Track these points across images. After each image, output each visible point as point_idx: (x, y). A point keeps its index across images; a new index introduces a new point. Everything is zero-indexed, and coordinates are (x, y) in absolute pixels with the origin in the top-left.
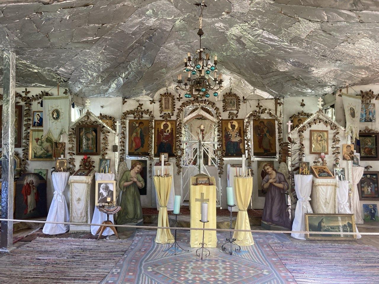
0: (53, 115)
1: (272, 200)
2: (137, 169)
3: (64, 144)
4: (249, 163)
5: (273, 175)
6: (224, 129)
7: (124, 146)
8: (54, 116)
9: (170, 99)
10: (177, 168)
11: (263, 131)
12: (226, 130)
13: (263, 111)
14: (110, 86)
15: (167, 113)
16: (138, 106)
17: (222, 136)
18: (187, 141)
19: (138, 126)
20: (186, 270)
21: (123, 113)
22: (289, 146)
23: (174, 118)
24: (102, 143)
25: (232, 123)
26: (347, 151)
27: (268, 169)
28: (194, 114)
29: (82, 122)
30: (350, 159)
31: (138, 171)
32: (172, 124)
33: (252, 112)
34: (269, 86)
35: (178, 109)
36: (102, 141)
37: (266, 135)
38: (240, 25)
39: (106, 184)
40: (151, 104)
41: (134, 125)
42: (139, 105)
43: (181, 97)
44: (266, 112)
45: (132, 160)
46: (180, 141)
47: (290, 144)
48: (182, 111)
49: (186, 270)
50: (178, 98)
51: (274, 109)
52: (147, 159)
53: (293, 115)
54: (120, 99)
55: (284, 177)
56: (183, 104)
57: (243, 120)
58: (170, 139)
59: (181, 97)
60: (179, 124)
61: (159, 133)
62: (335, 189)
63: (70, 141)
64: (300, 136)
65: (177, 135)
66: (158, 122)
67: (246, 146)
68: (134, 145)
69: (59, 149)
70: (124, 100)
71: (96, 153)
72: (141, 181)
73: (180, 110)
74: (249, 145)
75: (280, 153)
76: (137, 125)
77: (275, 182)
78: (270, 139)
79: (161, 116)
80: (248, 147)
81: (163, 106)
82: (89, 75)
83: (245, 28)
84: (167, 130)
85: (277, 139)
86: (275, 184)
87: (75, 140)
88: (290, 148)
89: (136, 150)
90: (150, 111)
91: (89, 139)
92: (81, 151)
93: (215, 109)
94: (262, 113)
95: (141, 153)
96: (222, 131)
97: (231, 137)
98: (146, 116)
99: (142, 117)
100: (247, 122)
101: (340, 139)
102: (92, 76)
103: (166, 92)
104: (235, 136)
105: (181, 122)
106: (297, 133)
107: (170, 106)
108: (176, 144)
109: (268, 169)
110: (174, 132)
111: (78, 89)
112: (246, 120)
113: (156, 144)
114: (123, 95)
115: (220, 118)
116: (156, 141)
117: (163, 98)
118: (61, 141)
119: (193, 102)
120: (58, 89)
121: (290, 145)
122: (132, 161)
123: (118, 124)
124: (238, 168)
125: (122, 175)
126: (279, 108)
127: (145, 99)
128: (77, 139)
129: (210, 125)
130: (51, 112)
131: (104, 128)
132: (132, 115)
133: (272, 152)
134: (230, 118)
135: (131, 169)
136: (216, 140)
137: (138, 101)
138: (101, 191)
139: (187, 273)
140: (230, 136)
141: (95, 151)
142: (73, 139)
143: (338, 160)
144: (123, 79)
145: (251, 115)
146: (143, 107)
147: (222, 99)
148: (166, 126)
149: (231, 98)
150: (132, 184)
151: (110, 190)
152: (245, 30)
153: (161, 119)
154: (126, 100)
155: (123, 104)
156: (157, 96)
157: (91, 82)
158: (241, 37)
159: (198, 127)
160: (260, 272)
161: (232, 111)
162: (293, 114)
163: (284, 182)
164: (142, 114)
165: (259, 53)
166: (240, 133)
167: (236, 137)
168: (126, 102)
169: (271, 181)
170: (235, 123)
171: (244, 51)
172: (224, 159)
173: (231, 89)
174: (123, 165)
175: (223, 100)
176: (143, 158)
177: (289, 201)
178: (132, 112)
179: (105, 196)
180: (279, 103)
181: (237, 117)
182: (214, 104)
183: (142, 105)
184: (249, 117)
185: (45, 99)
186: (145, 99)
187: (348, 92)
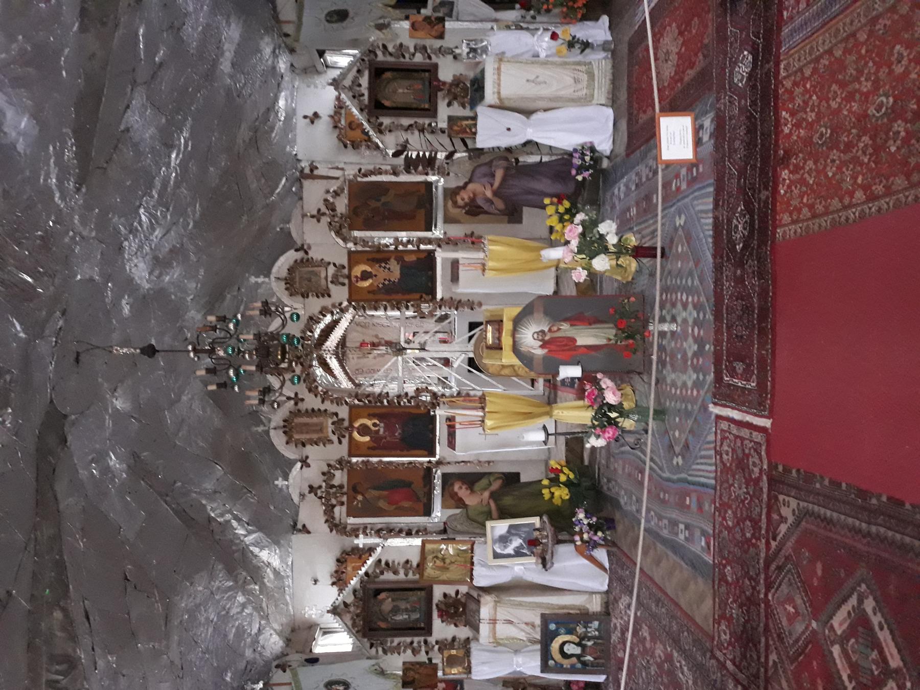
1: (532, 193)
4: (448, 242)
6: (371, 296)
13: (330, 207)
16: (316, 495)
17: (388, 301)
18: (395, 379)
19: (363, 495)
20: (679, 384)
21: (331, 531)
22: (414, 157)
23: (344, 412)
24: (406, 575)
25: (356, 277)
27: (463, 199)
28: (334, 363)
29: (354, 625)
30: (440, 25)
32: (359, 417)
33: (333, 234)
35: (323, 402)
37: (384, 204)
38: (130, 260)
39: (494, 542)
40: (309, 466)
42: (313, 494)
43: (293, 396)
44: (331, 200)
46: (399, 397)
49: (679, 384)
50: (296, 404)
51: (325, 182)
52: (439, 472)
53: (340, 139)
56: (310, 391)
57: (350, 253)
59: (293, 396)
61: (379, 446)
63: (397, 650)
65: (385, 403)
67: (410, 247)
68: (406, 504)
69: (417, 676)
70: (300, 531)
73: (325, 396)
74: (409, 242)
75: (427, 174)
76: (360, 498)
77: (492, 186)
79: (340, 442)
81: (315, 436)
82: (243, 611)
83: (134, 246)
85: (393, 178)
86: (497, 184)
87: (397, 640)
88: (418, 154)
89: (418, 500)
90: (326, 469)
91: (394, 606)
92: (422, 625)
94: (334, 210)
95: (425, 486)
97: (389, 281)
98: (340, 477)
99: (341, 487)
100: (355, 244)
102: (244, 606)
103: (281, 432)
105: (353, 394)
107: (315, 420)
108: (405, 407)
109: (463, 199)
110: (377, 411)
111: (275, 638)
112: (350, 245)
114: (287, 533)
115: (345, 304)
116: (398, 452)
117: (296, 436)
118: (401, 673)
120: (275, 685)
122: (444, 506)
123: (361, 541)
124: (461, 268)
125: (475, 525)
126: (322, 171)
127: (296, 481)
128: (396, 636)
129: (359, 329)
131: (370, 572)
132: (337, 510)
133: (423, 191)
134: (346, 281)
136: (397, 313)
137: (302, 496)
139: (684, 384)
142: (395, 644)
144: (250, 533)
145: (338, 233)
146: (315, 486)
147: (300, 298)
148: (364, 430)
150: (495, 501)
151: (508, 532)
152: (140, 247)
153: (345, 441)
154: (299, 526)
155: (309, 532)
156: (290, 453)
157: (259, 608)
158: (156, 258)
160: (680, 232)
161: (330, 279)
162: (336, 140)
164: (333, 486)
167: (389, 269)
168: (304, 526)
169: (489, 194)
170: (358, 270)
172: (439, 296)
174: (455, 523)
175: (303, 296)
176: (438, 482)
177: (534, 159)
179: (521, 541)
180: (312, 171)
183: (311, 487)
184: (345, 240)
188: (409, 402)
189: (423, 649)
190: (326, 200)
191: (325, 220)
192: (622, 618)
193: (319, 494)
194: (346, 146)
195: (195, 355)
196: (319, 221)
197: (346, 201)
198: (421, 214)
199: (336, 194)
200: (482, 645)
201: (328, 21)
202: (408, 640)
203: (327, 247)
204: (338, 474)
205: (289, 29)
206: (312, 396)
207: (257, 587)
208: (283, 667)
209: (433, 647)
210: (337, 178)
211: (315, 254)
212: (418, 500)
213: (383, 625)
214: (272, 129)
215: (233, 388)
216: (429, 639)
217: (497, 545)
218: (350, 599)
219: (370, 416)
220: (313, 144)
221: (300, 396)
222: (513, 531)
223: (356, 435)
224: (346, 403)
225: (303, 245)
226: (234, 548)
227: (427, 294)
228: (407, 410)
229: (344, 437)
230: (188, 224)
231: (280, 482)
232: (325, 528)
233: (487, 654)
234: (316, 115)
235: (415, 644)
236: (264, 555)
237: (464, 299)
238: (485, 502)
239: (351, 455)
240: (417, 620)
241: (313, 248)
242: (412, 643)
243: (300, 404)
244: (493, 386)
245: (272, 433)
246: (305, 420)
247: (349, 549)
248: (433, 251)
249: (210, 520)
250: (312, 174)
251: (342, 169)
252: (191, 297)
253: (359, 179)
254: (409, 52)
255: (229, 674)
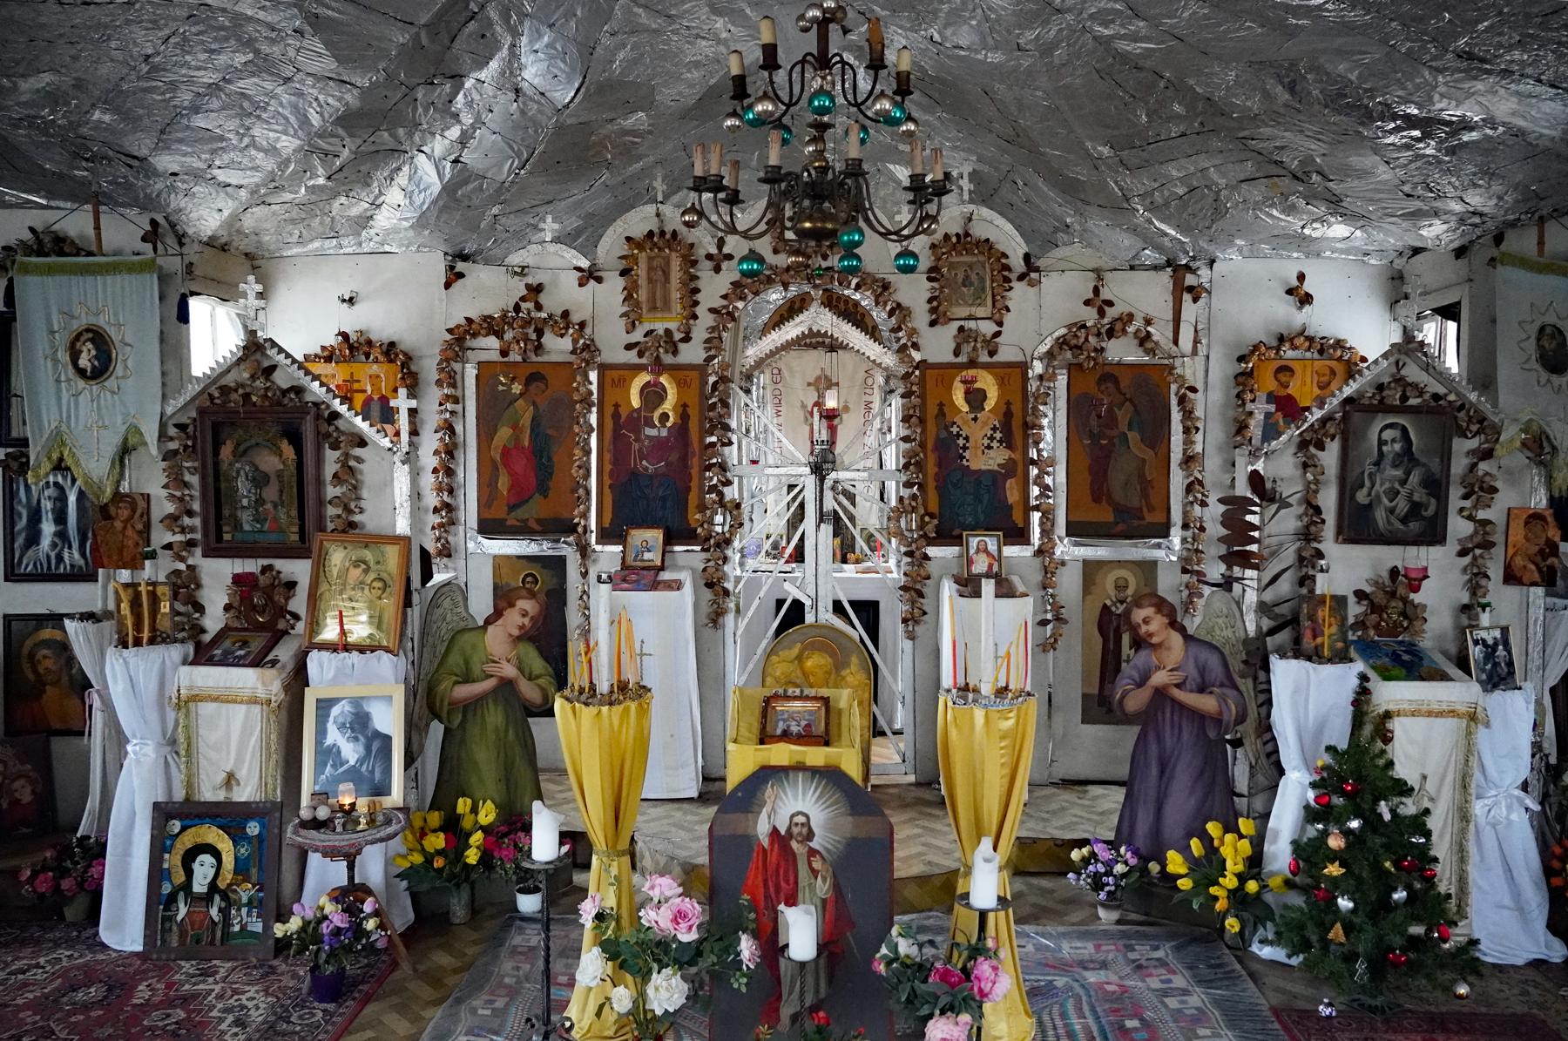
0: (75, 356)
2: (520, 620)
3: (141, 504)
5: (1169, 649)
6: (932, 410)
7: (451, 491)
8: (84, 362)
9: (676, 264)
10: (708, 594)
11: (1111, 420)
12: (941, 413)
14: (377, 197)
15: (661, 332)
16: (523, 299)
18: (765, 458)
19: (521, 395)
21: (450, 331)
22: (1249, 518)
23: (692, 353)
25: (974, 380)
26: (1527, 540)
27: (1146, 621)
29: (225, 390)
30: (1537, 577)
31: (521, 627)
32: (681, 385)
33: (1063, 331)
34: (1153, 208)
35: (712, 310)
36: (332, 491)
39: (357, 702)
40: (581, 285)
41: (501, 388)
43: (726, 250)
44: (1131, 329)
45: (495, 557)
46: (723, 467)
47: (1256, 505)
48: (734, 319)
50: (709, 257)
53: (1256, 347)
54: (436, 265)
55: (1225, 664)
58: (674, 457)
59: (726, 250)
60: (715, 383)
61: (622, 428)
62: (1469, 733)
63: (176, 480)
64: (1305, 466)
66: (615, 376)
67: (1035, 491)
68: (503, 483)
69: (118, 525)
70: (452, 268)
71: (300, 551)
72: (538, 677)
73: (725, 315)
76: (517, 388)
77: (1178, 686)
78: (1144, 461)
79: (629, 347)
80: (1042, 495)
81: (642, 295)
84: (656, 415)
85: (1176, 455)
86: (1176, 693)
87: (194, 480)
88: (1254, 527)
89: (512, 508)
90: (576, 318)
92: (227, 537)
93: (891, 314)
94: (1111, 333)
95: (538, 521)
96: (922, 421)
97: (965, 448)
98: (558, 346)
99: (539, 348)
100: (1041, 377)
101: (1498, 484)
102: (271, 150)
103: (653, 225)
104: (986, 442)
105: (728, 374)
106: (1292, 449)
107: (675, 295)
108: (702, 478)
109: (1146, 621)
113: (607, 481)
115: (917, 356)
116: (608, 467)
119: (785, 277)
121: (1256, 509)
122: (499, 562)
127: (552, 259)
128: (203, 479)
129: (862, 374)
130: (62, 340)
132: (492, 342)
133: (1150, 518)
134: (963, 359)
135: (489, 621)
137: (522, 271)
138: (334, 736)
140: (961, 442)
141: (295, 537)
142: (187, 477)
143: (1483, 582)
145: (1062, 343)
146: (543, 298)
148: (653, 395)
149: (966, 259)
150: (494, 691)
153: (631, 357)
154: (460, 266)
155: (448, 286)
156: (611, 246)
157: (274, 184)
159: (809, 384)
161: (971, 324)
163: (1222, 685)
165: (1123, 37)
166: (1006, 424)
167: (989, 447)
168: (461, 275)
169: (1159, 678)
170: (987, 382)
171: (1045, 23)
172: (932, 551)
173: (970, 220)
178: (492, 326)
179: (352, 762)
180: (1190, 289)
181: (992, 354)
182: (886, 286)
184: (1050, 355)
185: (26, 270)
186: (552, 259)
187: (1547, 248)
188: (713, 489)
189: (179, 538)
190: (1131, 317)
191: (1090, 316)
192: (220, 997)
193: (524, 305)
194: (1241, 359)
195: (814, 20)
196: (1087, 303)
197: (1130, 359)
198: (1105, 515)
199: (1144, 340)
200: (176, 669)
201: (1542, 329)
202: (196, 506)
203: (1035, 319)
204: (566, 344)
205: (1523, 242)
206: (725, 288)
207: (321, 181)
208: (152, 235)
209: (183, 560)
210: (1176, 342)
211: (1019, 294)
212: (512, 508)
213: (226, 451)
214: (1291, 210)
215: (734, 114)
216: (198, 551)
217: (348, 708)
218: (281, 379)
219: (683, 410)
220: (1246, 290)
221: (725, 265)
222: (375, 746)
223: (644, 378)
224: (709, 359)
225: (1037, 270)
226: (401, 131)
227: (938, 529)
228: (694, 484)
229: (641, 354)
230: (1106, 24)
231: (550, 227)
232: (458, 319)
233: (153, 685)
234: (1306, 299)
235: (187, 521)
236: (394, 196)
237: (927, 604)
238: (489, 668)
239: (603, 369)
240: (237, 526)
241: (1032, 291)
242: (190, 513)
243: (709, 264)
244: (744, 664)
245: (650, 209)
246: (676, 274)
247: (413, 368)
248: (1027, 542)
249: (457, 78)
250: (1185, 288)
251: (1195, 352)
252: (937, 37)
253: (1174, 387)
254: (1475, 507)
255: (107, 118)
